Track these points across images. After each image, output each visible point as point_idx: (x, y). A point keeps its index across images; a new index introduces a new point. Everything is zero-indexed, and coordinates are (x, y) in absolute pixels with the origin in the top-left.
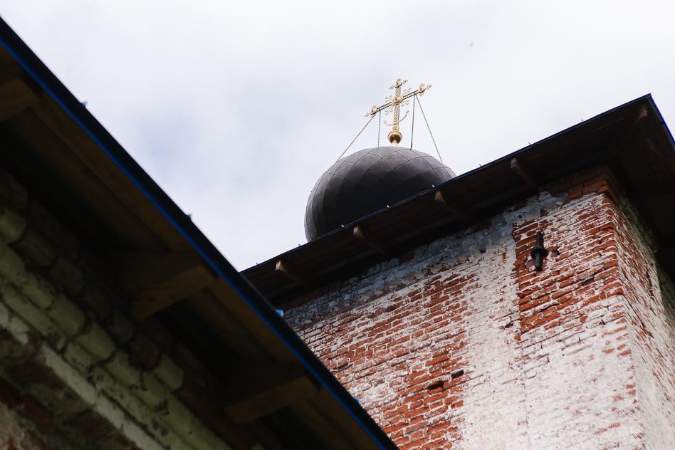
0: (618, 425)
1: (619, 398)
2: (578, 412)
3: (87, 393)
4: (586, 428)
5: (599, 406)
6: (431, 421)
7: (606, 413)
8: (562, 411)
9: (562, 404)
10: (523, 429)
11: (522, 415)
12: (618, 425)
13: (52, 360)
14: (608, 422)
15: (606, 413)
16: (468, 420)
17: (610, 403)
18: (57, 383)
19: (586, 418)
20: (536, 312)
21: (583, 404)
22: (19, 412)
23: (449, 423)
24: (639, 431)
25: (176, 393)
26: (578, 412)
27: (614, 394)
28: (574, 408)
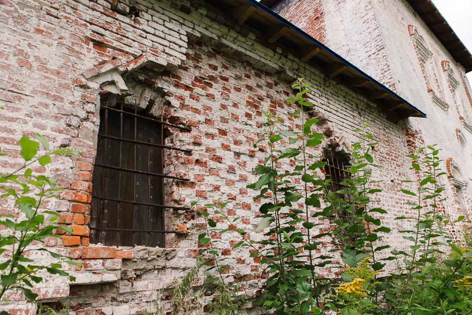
2: (356, 14)
3: (235, 47)
5: (362, 10)
14: (365, 14)
18: (227, 46)
19: (359, 15)
24: (373, 14)
25: (255, 40)
26: (356, 14)
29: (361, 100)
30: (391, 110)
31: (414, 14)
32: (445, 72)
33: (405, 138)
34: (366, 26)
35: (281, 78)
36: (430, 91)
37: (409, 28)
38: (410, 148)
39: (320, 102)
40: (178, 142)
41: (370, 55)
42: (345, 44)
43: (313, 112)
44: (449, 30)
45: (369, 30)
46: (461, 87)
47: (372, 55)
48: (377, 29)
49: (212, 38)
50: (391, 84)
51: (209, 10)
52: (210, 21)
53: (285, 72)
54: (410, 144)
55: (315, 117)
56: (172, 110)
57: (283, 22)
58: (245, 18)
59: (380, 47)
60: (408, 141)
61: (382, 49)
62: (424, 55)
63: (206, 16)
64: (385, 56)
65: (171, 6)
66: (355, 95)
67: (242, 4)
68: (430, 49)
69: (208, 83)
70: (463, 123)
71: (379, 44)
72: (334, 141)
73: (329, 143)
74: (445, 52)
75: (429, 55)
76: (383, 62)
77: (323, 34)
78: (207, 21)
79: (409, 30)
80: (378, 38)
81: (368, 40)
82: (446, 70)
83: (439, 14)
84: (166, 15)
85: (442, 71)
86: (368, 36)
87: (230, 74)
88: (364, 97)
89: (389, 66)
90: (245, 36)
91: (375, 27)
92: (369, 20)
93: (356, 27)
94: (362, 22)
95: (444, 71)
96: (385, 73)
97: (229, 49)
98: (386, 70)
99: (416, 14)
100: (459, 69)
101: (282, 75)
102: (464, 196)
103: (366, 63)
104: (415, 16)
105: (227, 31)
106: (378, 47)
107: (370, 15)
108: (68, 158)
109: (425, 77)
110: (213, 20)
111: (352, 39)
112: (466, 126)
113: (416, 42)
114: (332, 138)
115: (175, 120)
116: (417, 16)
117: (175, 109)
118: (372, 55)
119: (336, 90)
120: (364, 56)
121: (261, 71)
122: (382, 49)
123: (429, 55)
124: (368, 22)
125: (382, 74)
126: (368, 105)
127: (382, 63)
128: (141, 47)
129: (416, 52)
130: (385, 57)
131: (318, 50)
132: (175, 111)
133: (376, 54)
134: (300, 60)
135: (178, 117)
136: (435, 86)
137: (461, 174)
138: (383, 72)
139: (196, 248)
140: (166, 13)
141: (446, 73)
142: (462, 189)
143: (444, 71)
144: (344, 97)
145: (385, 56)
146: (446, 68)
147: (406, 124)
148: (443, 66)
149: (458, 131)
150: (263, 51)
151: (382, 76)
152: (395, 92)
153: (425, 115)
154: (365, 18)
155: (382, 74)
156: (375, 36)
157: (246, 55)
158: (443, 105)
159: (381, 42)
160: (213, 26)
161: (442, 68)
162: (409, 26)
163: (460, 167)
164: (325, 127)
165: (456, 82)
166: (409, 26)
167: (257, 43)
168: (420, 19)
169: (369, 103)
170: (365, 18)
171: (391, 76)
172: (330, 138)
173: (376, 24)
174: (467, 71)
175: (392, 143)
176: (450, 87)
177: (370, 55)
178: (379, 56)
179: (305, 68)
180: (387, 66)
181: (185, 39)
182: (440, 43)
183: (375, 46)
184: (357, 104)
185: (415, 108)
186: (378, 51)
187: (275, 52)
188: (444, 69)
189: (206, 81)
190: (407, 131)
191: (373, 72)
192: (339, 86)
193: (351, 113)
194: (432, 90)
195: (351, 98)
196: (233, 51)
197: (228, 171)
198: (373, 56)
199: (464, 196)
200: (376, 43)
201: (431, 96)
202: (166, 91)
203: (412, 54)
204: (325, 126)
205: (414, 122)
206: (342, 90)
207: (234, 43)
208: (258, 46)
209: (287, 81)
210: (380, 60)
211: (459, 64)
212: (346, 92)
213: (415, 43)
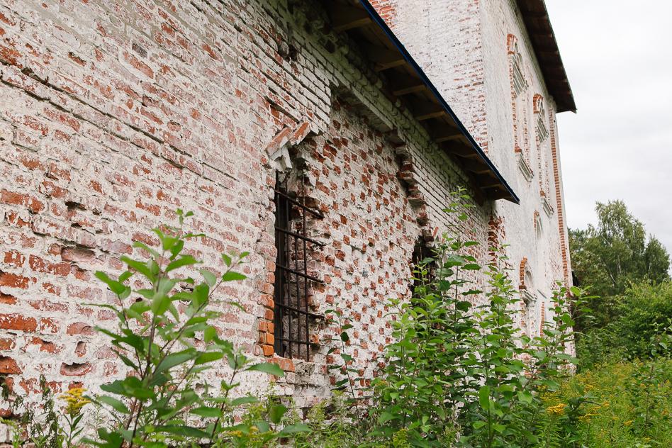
0: (469, 18)
1: (471, 5)
2: (452, 10)
3: (361, 98)
4: (455, 18)
5: (461, 8)
6: (382, 4)
7: (464, 12)
8: (444, 9)
9: (445, 5)
10: (426, 13)
11: (426, 7)
12: (469, 18)
13: (356, 92)
14: (465, 17)
15: (464, 12)
16: (400, 6)
17: (466, 7)
18: (355, 97)
19: (455, 13)
20: (591, 229)
21: (454, 6)
22: (345, 108)
23: (390, 7)
24: (479, 22)
25: (380, 90)
26: (452, 10)
27: (469, 3)
28: (450, 7)
29: (455, 172)
30: (482, 188)
31: (515, 11)
32: (536, 114)
33: (488, 228)
34: (462, 37)
35: (391, 141)
36: (518, 150)
37: (508, 40)
38: (492, 244)
39: (426, 181)
40: (312, 232)
41: (461, 87)
42: (425, 51)
43: (413, 191)
44: (553, 47)
45: (467, 46)
46: (548, 140)
47: (464, 87)
48: (479, 50)
49: (345, 87)
50: (483, 141)
51: (350, 49)
52: (347, 62)
53: (397, 133)
54: (492, 237)
55: (413, 196)
56: (308, 188)
57: (421, 77)
58: (386, 67)
59: (477, 79)
60: (491, 233)
61: (480, 83)
62: (518, 83)
63: (346, 56)
64: (482, 96)
65: (319, 42)
66: (451, 165)
67: (388, 49)
68: (526, 78)
69: (333, 148)
70: (543, 201)
71: (476, 73)
72: (428, 233)
73: (421, 234)
74: (540, 81)
75: (523, 86)
76: (478, 105)
77: (391, 18)
78: (345, 63)
79: (508, 44)
80: (478, 63)
81: (462, 61)
82: (538, 112)
83: (548, 21)
84: (314, 56)
85: (532, 111)
86: (463, 54)
87: (350, 135)
88: (459, 167)
89: (484, 114)
90: (372, 84)
91: (476, 45)
92: (470, 30)
93: (447, 32)
94: (458, 28)
95: (535, 113)
96: (478, 123)
97: (354, 100)
98: (481, 118)
99: (518, 11)
100: (550, 106)
101: (391, 136)
102: (531, 315)
103: (452, 96)
104: (517, 15)
105: (359, 77)
106: (474, 78)
107: (473, 23)
108: (260, 256)
109: (515, 126)
110: (351, 62)
111: (438, 48)
112: (545, 206)
113: (514, 65)
114: (426, 228)
115: (311, 201)
116: (519, 15)
117: (312, 187)
118: (464, 87)
119: (435, 158)
120: (452, 84)
121: (375, 130)
122: (480, 83)
123: (523, 86)
124: (468, 32)
125: (473, 122)
126: (460, 178)
127: (476, 105)
128: (301, 108)
129: (511, 82)
130: (482, 99)
131: (442, 113)
132: (311, 190)
133: (470, 88)
134: (414, 117)
135: (313, 199)
136: (522, 139)
137: (532, 283)
138: (475, 119)
139: (325, 364)
140: (315, 52)
141: (537, 115)
142: (530, 305)
143: (535, 113)
144: (440, 167)
145: (482, 96)
146: (538, 110)
147: (492, 208)
148: (534, 105)
149: (537, 214)
150: (384, 104)
151: (472, 125)
152: (486, 155)
153: (518, 200)
154: (465, 24)
155: (473, 122)
156: (474, 59)
157: (369, 110)
158: (527, 173)
159: (480, 72)
160: (348, 70)
161: (533, 107)
162: (510, 36)
163: (533, 274)
164: (421, 211)
165: (545, 132)
166: (510, 36)
167: (383, 96)
168: (521, 20)
169: (462, 176)
170: (465, 24)
171: (485, 131)
172: (423, 228)
173: (479, 40)
174: (559, 111)
175: (475, 236)
176: (537, 140)
177: (461, 87)
178: (474, 93)
179: (415, 128)
180: (482, 113)
181: (329, 91)
182: (536, 62)
183: (471, 74)
184: (449, 177)
185: (511, 190)
186: (474, 85)
187: (394, 105)
188: (535, 108)
189: (332, 146)
190: (492, 219)
191: (463, 111)
192: (439, 152)
193: (444, 190)
194: (520, 150)
195: (446, 169)
196: (357, 103)
197: (347, 272)
198: (465, 90)
199: (531, 315)
200: (472, 70)
201: (518, 159)
202: (307, 164)
203: (506, 83)
204: (421, 211)
205: (501, 205)
206: (441, 157)
207: (361, 93)
208: (381, 99)
209: (393, 143)
210: (475, 99)
211: (551, 99)
212: (444, 161)
213: (512, 68)
